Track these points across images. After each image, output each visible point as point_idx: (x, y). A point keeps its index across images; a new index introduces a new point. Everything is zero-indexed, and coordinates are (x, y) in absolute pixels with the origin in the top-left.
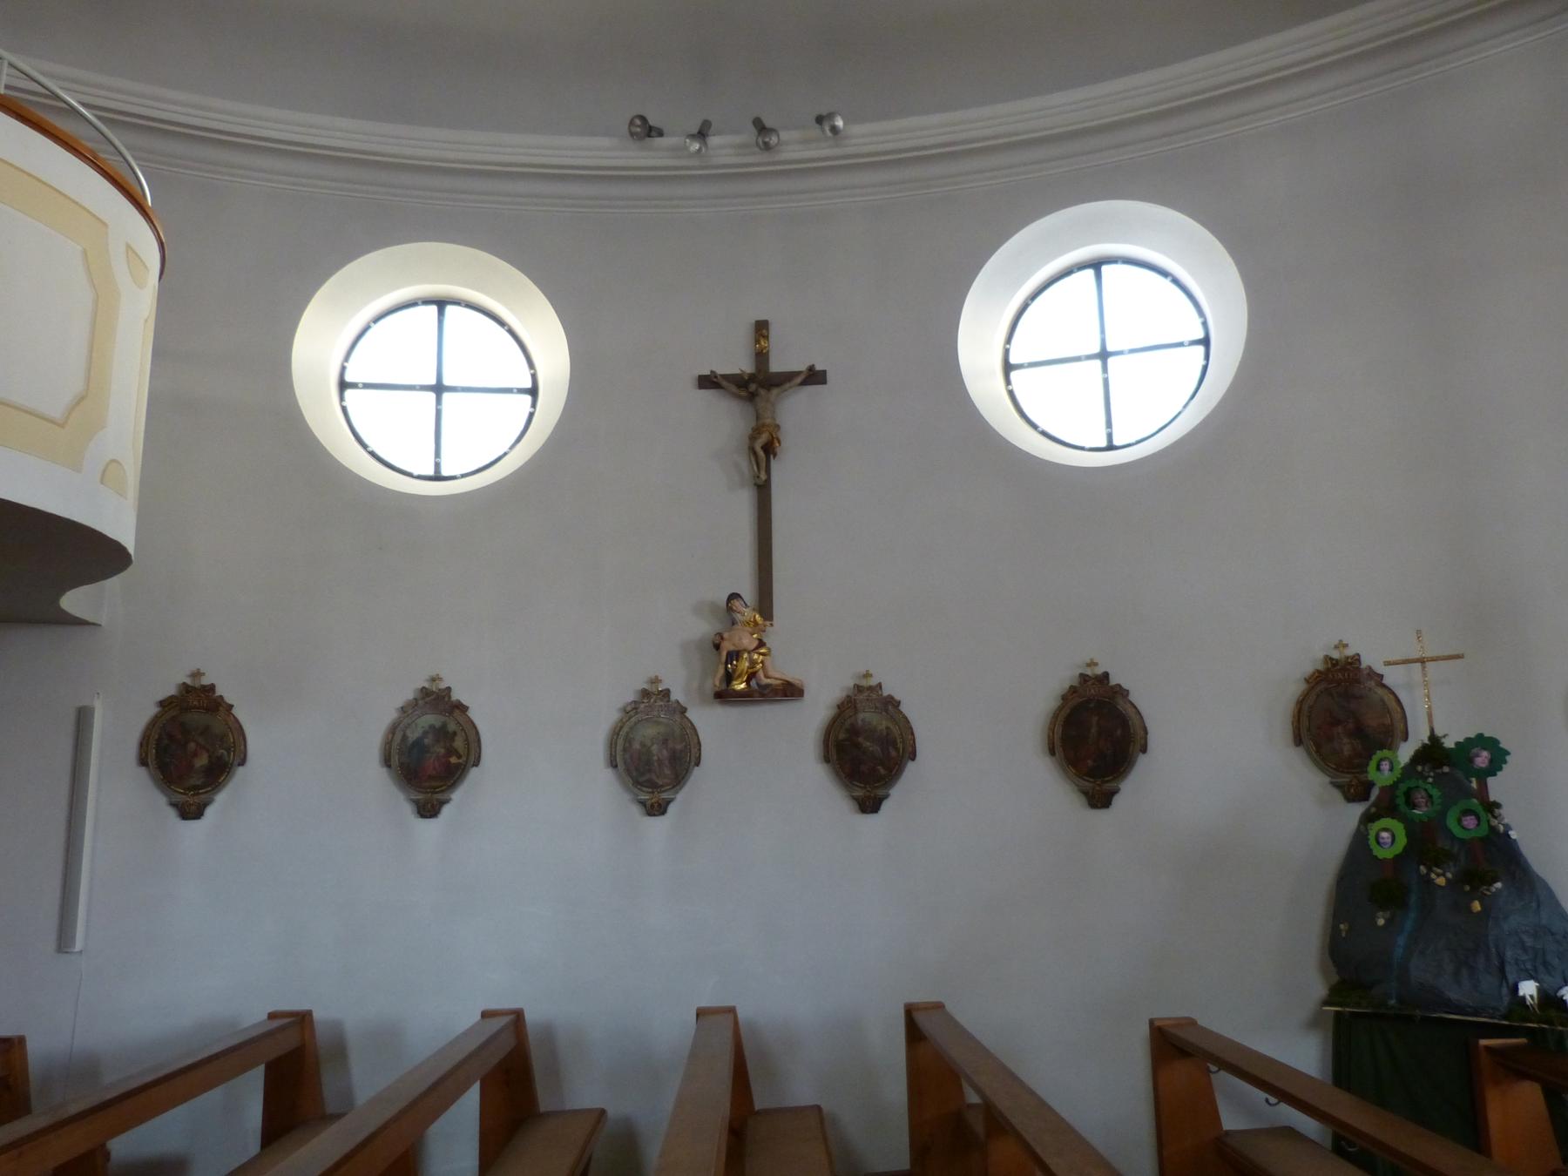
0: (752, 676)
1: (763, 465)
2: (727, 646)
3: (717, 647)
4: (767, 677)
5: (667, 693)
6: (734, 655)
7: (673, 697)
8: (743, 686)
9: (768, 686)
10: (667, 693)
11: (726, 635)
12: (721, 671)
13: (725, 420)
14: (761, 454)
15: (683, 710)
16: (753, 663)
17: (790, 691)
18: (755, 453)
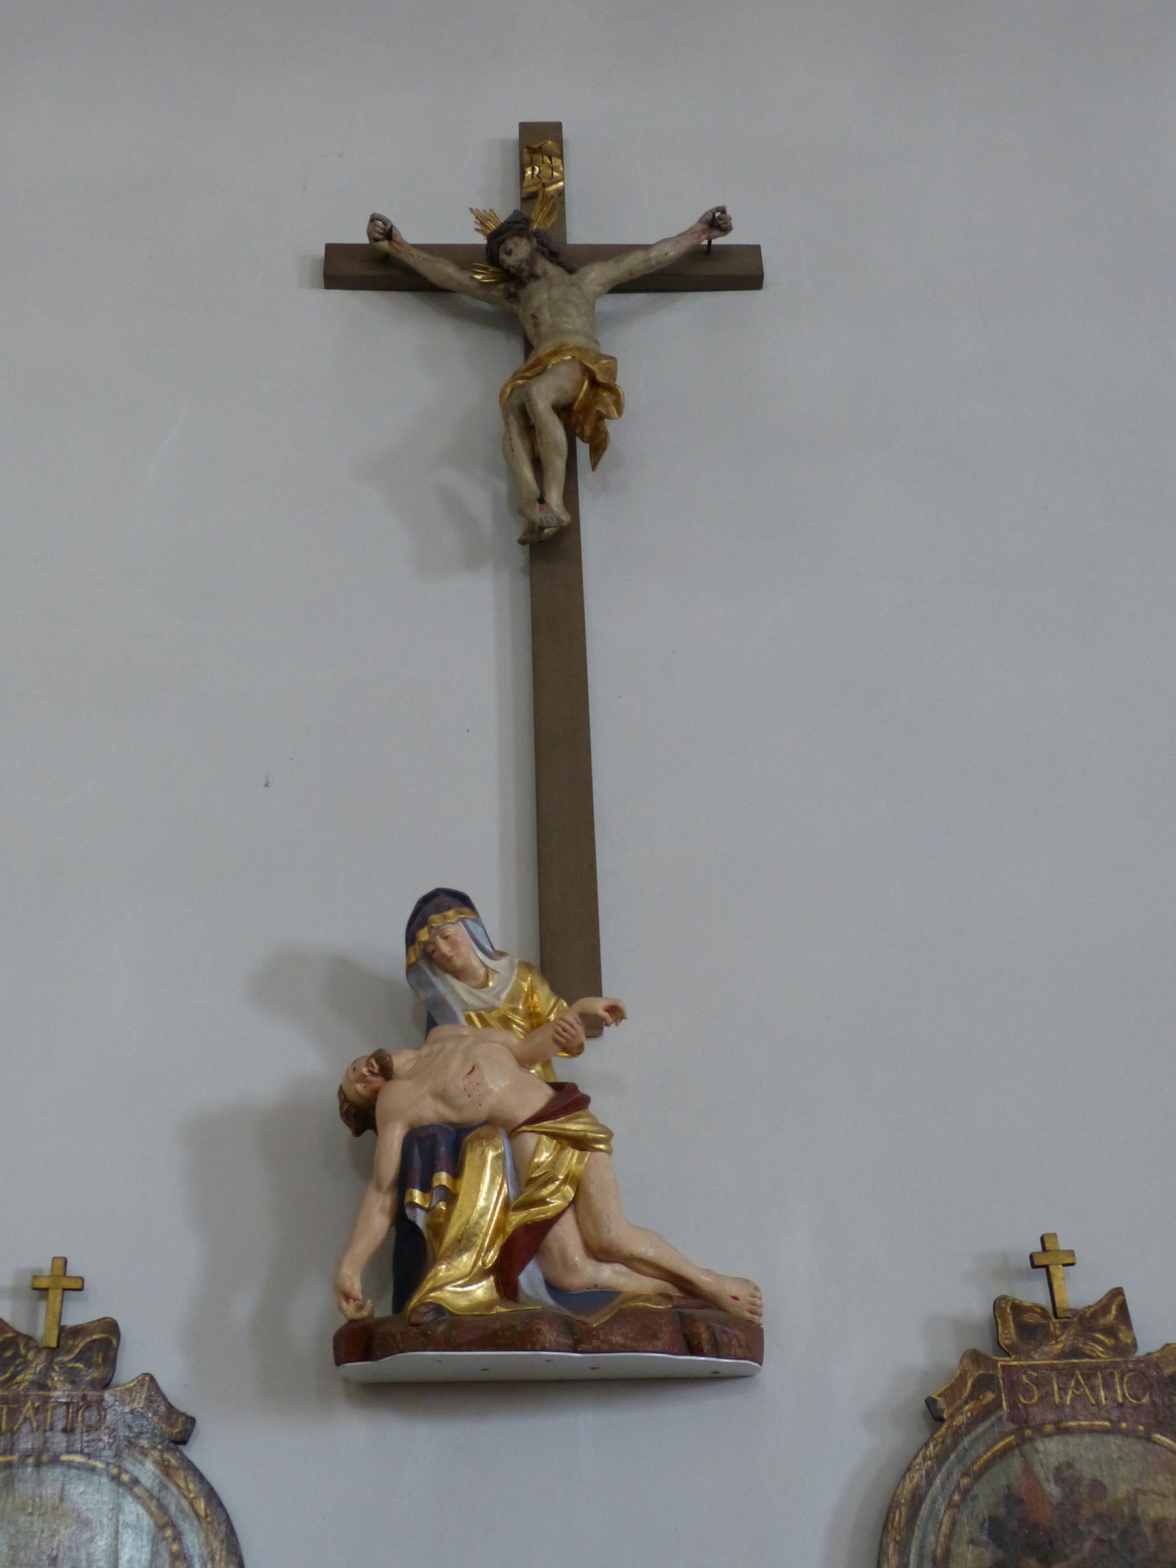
0: (522, 1245)
1: (557, 465)
2: (407, 1105)
3: (361, 1116)
4: (601, 1253)
5: (103, 1342)
6: (438, 1150)
7: (131, 1365)
8: (482, 1290)
9: (602, 1296)
10: (103, 1342)
11: (402, 1061)
12: (376, 1223)
13: (423, 377)
14: (556, 431)
15: (178, 1431)
16: (525, 1184)
17: (700, 1332)
18: (529, 427)
